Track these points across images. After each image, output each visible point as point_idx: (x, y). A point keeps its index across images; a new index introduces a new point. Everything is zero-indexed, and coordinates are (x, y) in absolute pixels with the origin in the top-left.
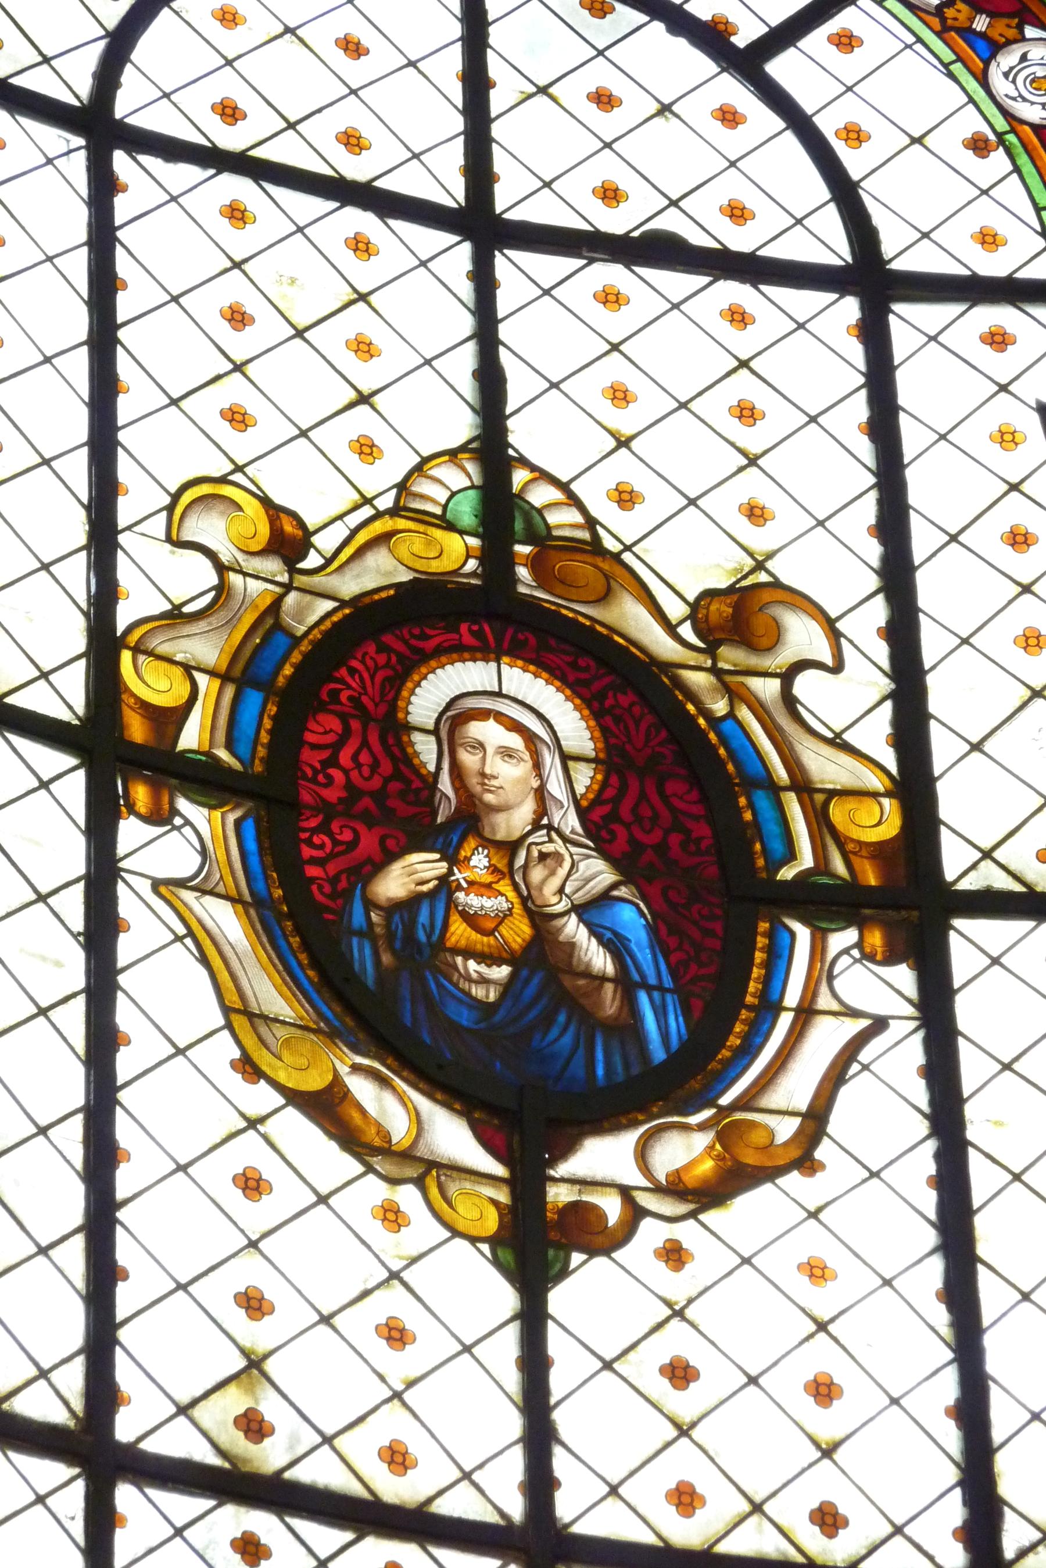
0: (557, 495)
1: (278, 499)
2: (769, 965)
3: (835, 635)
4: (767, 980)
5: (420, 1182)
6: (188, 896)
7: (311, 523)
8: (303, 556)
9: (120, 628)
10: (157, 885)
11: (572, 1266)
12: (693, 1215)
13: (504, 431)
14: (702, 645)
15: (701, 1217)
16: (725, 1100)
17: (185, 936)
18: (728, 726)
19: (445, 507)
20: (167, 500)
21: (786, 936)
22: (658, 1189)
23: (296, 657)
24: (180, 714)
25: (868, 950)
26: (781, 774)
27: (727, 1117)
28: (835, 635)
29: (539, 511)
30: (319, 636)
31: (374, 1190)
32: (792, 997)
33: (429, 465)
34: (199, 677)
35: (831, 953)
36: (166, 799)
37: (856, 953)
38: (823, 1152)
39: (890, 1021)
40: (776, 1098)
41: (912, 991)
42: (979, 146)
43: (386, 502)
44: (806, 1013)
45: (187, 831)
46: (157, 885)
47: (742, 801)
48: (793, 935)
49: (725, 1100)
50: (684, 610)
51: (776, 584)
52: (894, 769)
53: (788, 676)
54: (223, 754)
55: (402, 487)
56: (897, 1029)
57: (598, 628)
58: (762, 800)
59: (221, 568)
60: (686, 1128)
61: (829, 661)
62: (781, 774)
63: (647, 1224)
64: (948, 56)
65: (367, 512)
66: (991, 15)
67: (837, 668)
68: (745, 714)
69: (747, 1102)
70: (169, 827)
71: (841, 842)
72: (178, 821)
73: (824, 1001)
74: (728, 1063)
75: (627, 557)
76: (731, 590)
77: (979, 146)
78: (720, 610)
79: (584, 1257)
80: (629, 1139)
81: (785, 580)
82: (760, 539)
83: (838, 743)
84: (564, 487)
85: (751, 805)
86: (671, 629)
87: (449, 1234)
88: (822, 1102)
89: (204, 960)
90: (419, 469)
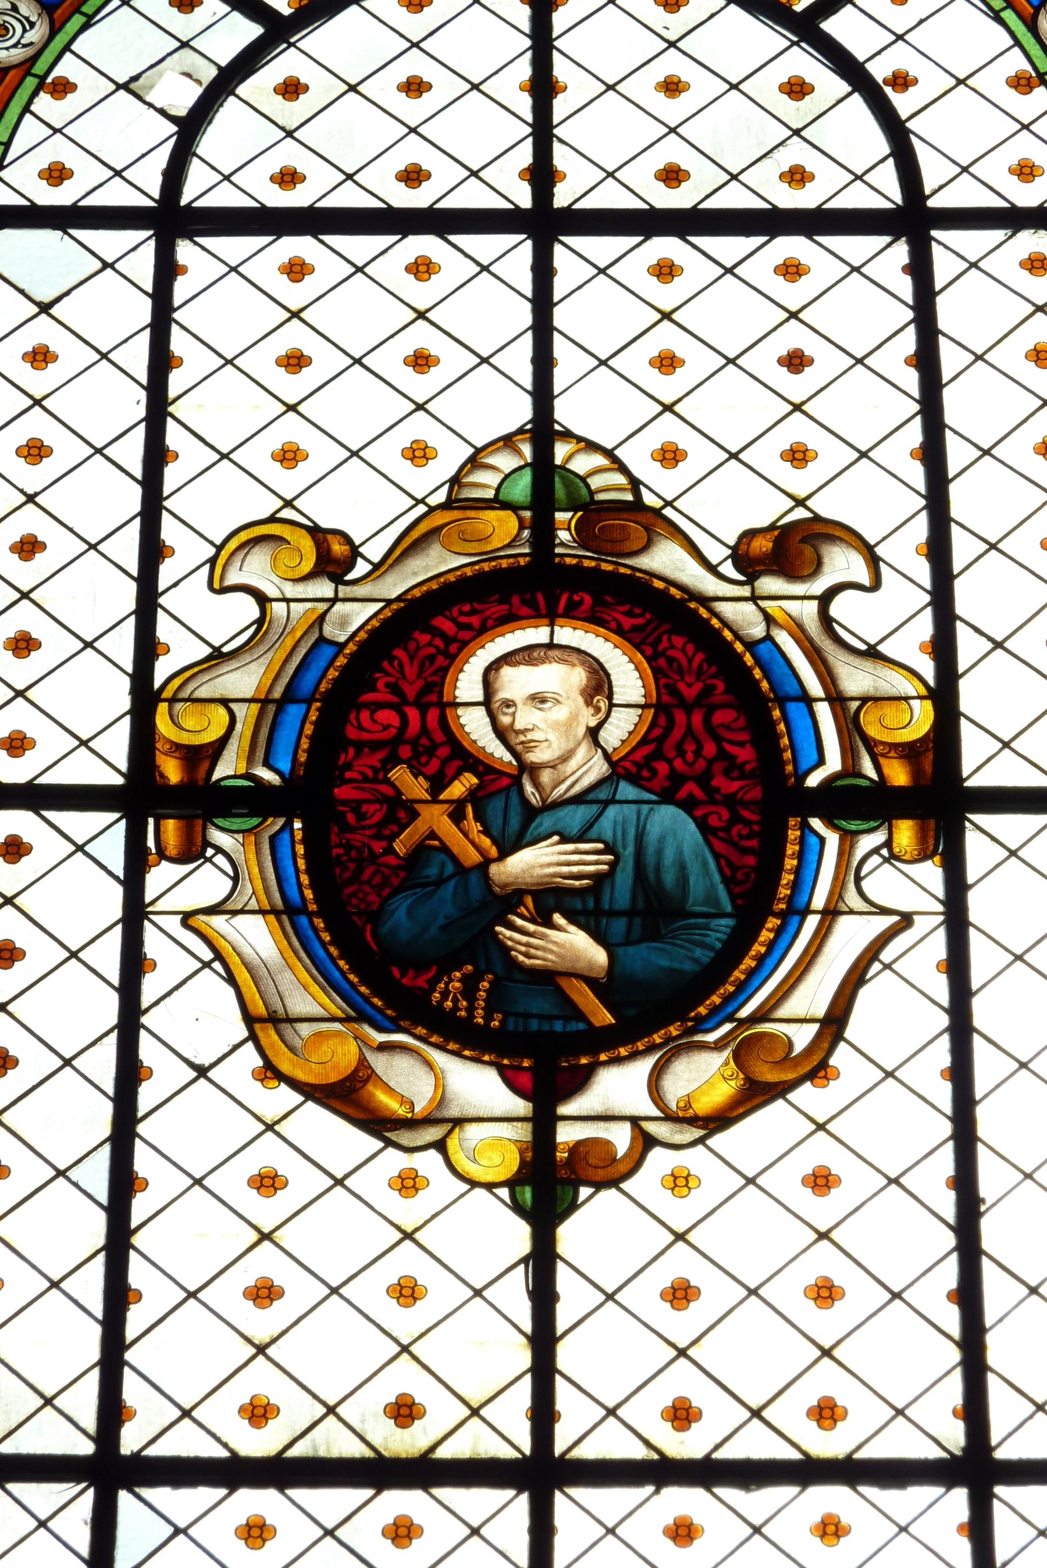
1: (324, 524)
3: (873, 561)
5: (440, 1146)
6: (218, 922)
9: (157, 683)
10: (187, 918)
11: (581, 1199)
12: (701, 1141)
13: (551, 409)
14: (742, 578)
15: (708, 1142)
16: (745, 1012)
17: (212, 961)
18: (764, 649)
19: (498, 489)
20: (211, 551)
22: (669, 1117)
24: (219, 746)
25: (896, 850)
26: (814, 687)
27: (747, 1029)
28: (873, 561)
29: (583, 479)
30: (355, 648)
31: (394, 1161)
32: (819, 901)
33: (483, 454)
37: (885, 852)
38: (841, 1057)
39: (915, 917)
40: (794, 1006)
43: (440, 497)
44: (831, 913)
45: (220, 860)
46: (187, 918)
47: (777, 713)
48: (822, 841)
49: (745, 1012)
51: (817, 518)
52: (931, 682)
53: (825, 599)
55: (455, 481)
57: (673, 591)
59: (262, 599)
60: (703, 1046)
61: (865, 580)
62: (814, 687)
63: (656, 1154)
64: (77, 21)
65: (422, 509)
67: (876, 585)
68: (783, 638)
70: (202, 860)
71: (870, 745)
72: (210, 852)
73: (852, 899)
75: (668, 512)
76: (772, 527)
78: (763, 545)
79: (591, 1190)
80: (644, 1066)
81: (824, 514)
82: (800, 481)
83: (872, 653)
84: (609, 454)
85: (785, 717)
86: (712, 569)
87: (467, 1187)
88: (842, 1003)
89: (231, 979)
90: (474, 462)
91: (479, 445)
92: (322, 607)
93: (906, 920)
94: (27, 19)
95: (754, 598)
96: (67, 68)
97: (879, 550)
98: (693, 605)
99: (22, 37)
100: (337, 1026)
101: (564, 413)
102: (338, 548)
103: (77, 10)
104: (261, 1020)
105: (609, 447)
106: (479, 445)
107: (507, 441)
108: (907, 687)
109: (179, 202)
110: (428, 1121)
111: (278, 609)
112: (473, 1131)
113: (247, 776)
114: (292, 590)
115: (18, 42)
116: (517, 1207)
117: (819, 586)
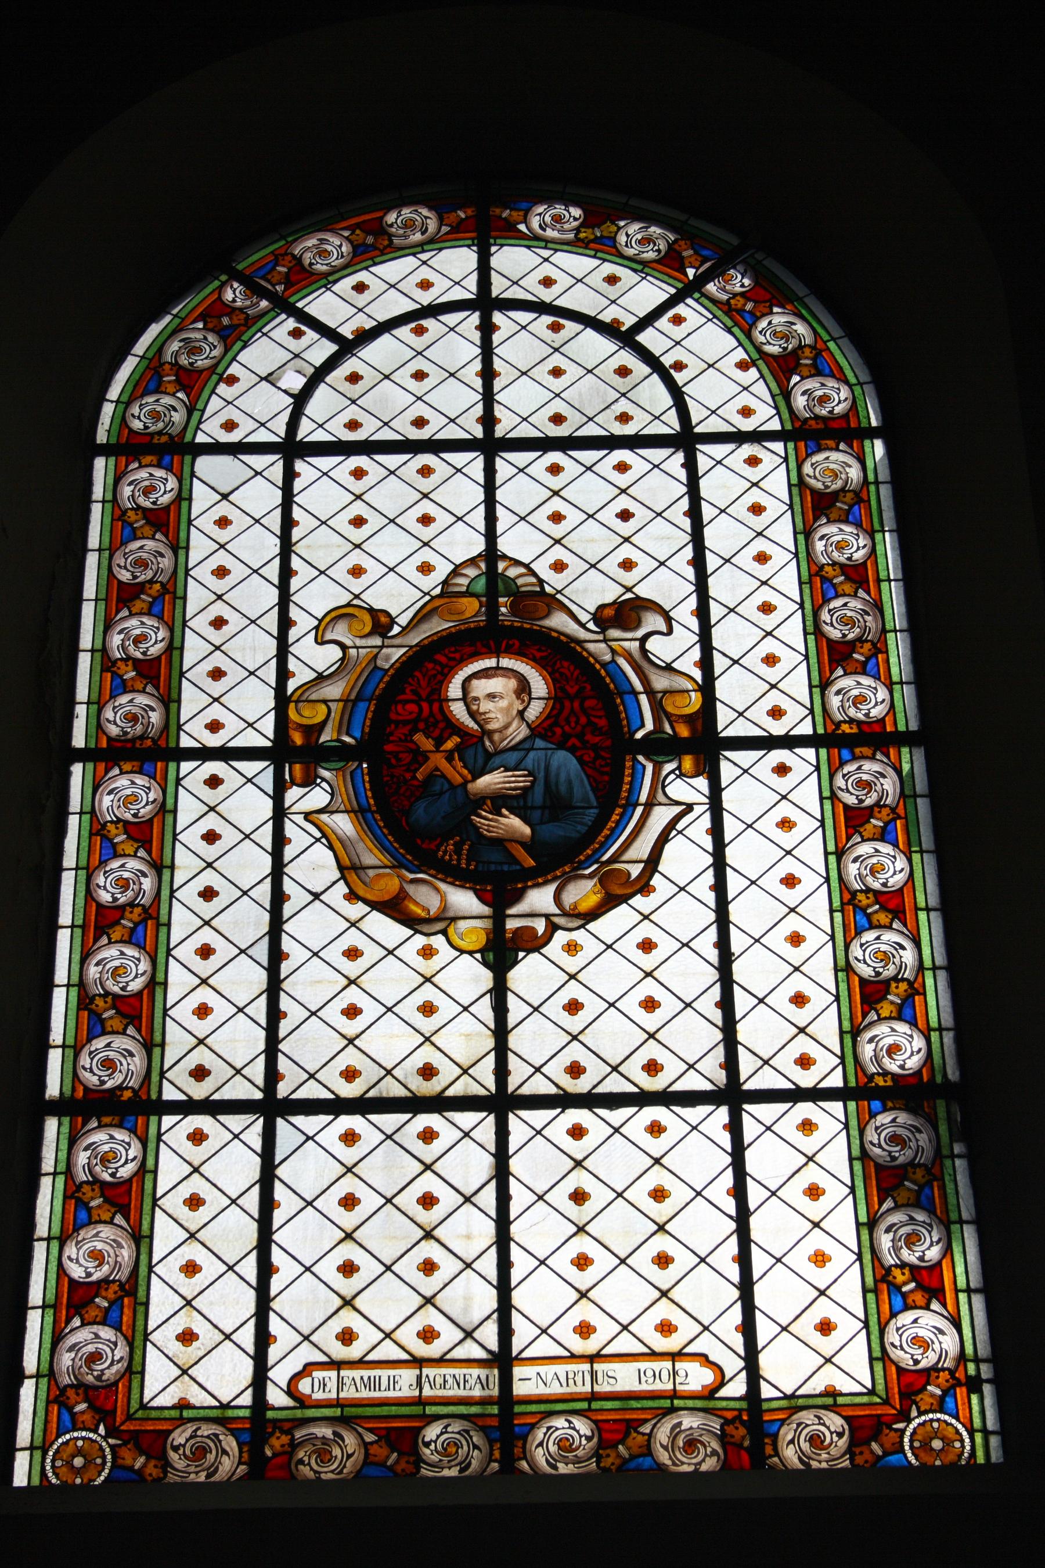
0: (523, 570)
2: (633, 775)
4: (630, 791)
5: (444, 932)
6: (324, 817)
7: (394, 614)
8: (391, 628)
10: (307, 816)
12: (583, 926)
13: (495, 544)
21: (640, 767)
22: (565, 914)
28: (669, 620)
31: (420, 941)
34: (330, 704)
35: (664, 773)
36: (312, 768)
37: (677, 772)
38: (656, 880)
40: (631, 854)
41: (706, 791)
42: (743, 366)
43: (438, 591)
44: (649, 805)
45: (324, 785)
46: (307, 816)
47: (618, 701)
50: (590, 617)
51: (638, 598)
54: (347, 739)
55: (445, 583)
56: (698, 810)
58: (629, 699)
59: (343, 647)
60: (584, 877)
61: (664, 629)
66: (755, 302)
67: (670, 632)
69: (615, 859)
71: (669, 716)
72: (319, 781)
73: (660, 797)
74: (607, 837)
75: (559, 596)
76: (614, 602)
77: (743, 366)
78: (609, 612)
80: (551, 889)
84: (527, 566)
85: (623, 702)
86: (583, 626)
89: (331, 847)
92: (376, 650)
93: (689, 808)
94: (123, 1141)
95: (605, 641)
96: (234, 369)
98: (573, 645)
99: (113, 1355)
100: (388, 871)
101: (504, 545)
102: (383, 619)
103: (239, 339)
104: (348, 868)
106: (458, 563)
107: (472, 562)
110: (437, 919)
111: (353, 652)
112: (463, 925)
114: (359, 642)
116: (485, 963)
117: (640, 633)
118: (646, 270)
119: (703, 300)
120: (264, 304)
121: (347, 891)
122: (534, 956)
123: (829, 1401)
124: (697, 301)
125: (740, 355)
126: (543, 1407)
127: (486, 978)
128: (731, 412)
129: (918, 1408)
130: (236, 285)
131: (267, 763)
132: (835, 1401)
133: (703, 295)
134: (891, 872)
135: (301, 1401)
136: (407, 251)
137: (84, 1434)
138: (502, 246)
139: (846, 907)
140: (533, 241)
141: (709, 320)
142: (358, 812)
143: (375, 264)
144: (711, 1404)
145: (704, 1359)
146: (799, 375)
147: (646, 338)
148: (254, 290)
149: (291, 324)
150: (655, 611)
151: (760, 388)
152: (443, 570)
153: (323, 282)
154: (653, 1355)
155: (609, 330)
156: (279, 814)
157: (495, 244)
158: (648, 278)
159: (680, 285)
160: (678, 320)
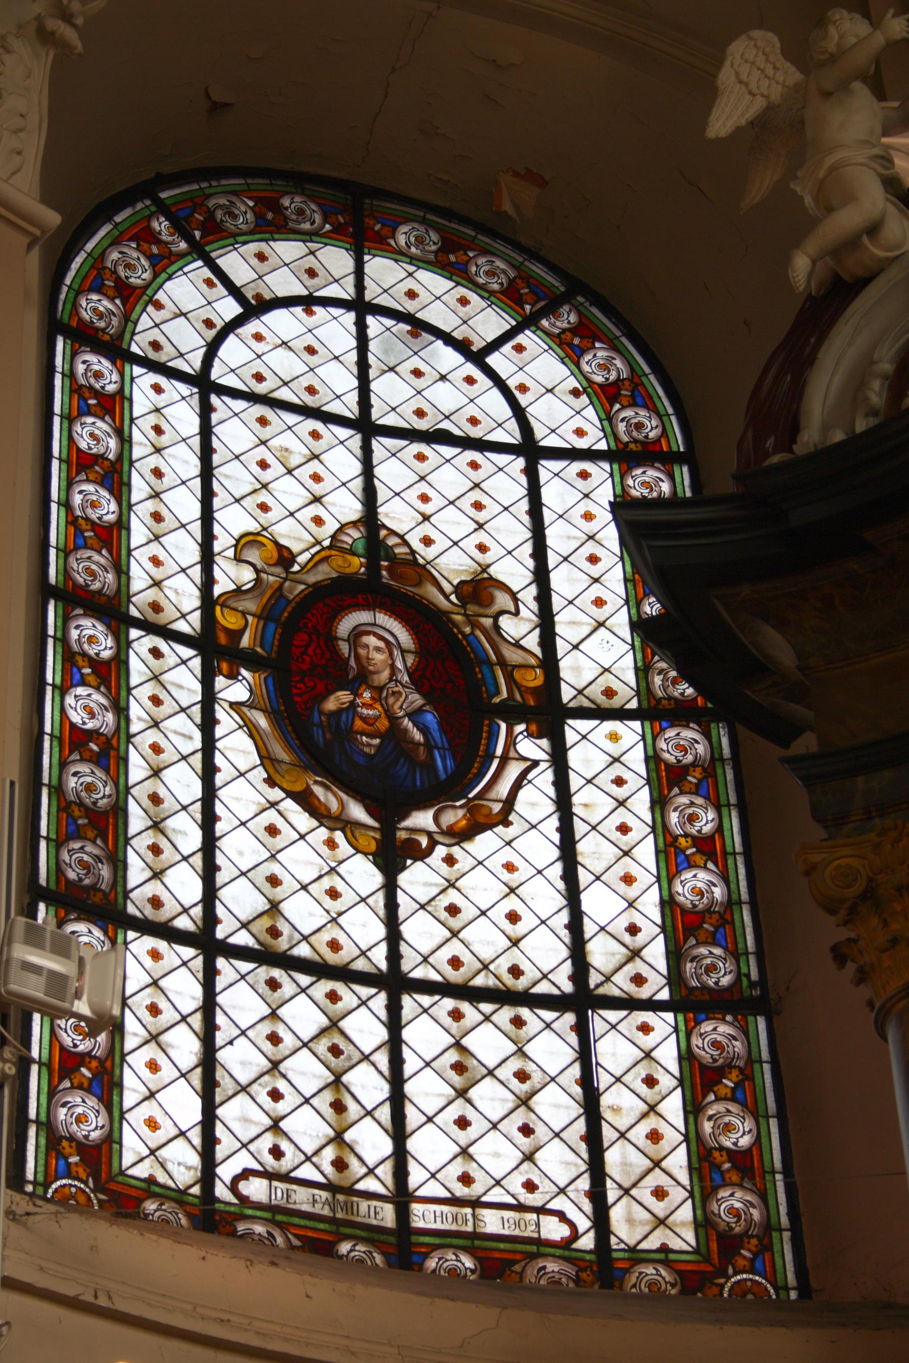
4: (488, 745)
8: (292, 566)
12: (458, 844)
16: (471, 795)
22: (443, 833)
23: (289, 609)
24: (240, 633)
28: (516, 600)
32: (499, 751)
37: (525, 734)
42: (575, 393)
44: (505, 760)
45: (244, 682)
47: (477, 670)
49: (471, 795)
51: (491, 578)
53: (496, 617)
54: (259, 650)
55: (334, 537)
56: (543, 766)
59: (257, 571)
61: (513, 610)
71: (519, 687)
72: (240, 678)
73: (512, 754)
75: (428, 566)
77: (575, 393)
78: (468, 589)
83: (517, 645)
84: (402, 537)
85: (481, 671)
86: (447, 597)
91: (344, 521)
93: (535, 763)
96: (160, 296)
97: (519, 596)
105: (402, 533)
107: (354, 524)
108: (533, 661)
109: (703, 123)
113: (253, 649)
115: (97, 1126)
118: (492, 299)
119: (539, 332)
120: (183, 245)
121: (266, 776)
122: (419, 864)
123: (661, 1256)
124: (534, 332)
125: (573, 383)
126: (436, 1241)
127: (378, 879)
128: (567, 431)
129: (734, 1268)
130: (162, 219)
131: (379, 422)
132: (667, 1256)
133: (539, 328)
134: (704, 821)
135: (244, 1200)
136: (298, 237)
137: (76, 1183)
138: (374, 256)
139: (668, 849)
140: (398, 255)
141: (545, 351)
142: (272, 714)
143: (274, 240)
144: (567, 1253)
145: (561, 1216)
146: (620, 403)
147: (493, 360)
148: (180, 228)
149: (207, 273)
150: (506, 592)
151: (590, 412)
152: (331, 527)
153: (231, 240)
154: (520, 1208)
155: (462, 347)
156: (209, 699)
157: (369, 254)
158: (493, 306)
159: (520, 319)
160: (519, 349)
